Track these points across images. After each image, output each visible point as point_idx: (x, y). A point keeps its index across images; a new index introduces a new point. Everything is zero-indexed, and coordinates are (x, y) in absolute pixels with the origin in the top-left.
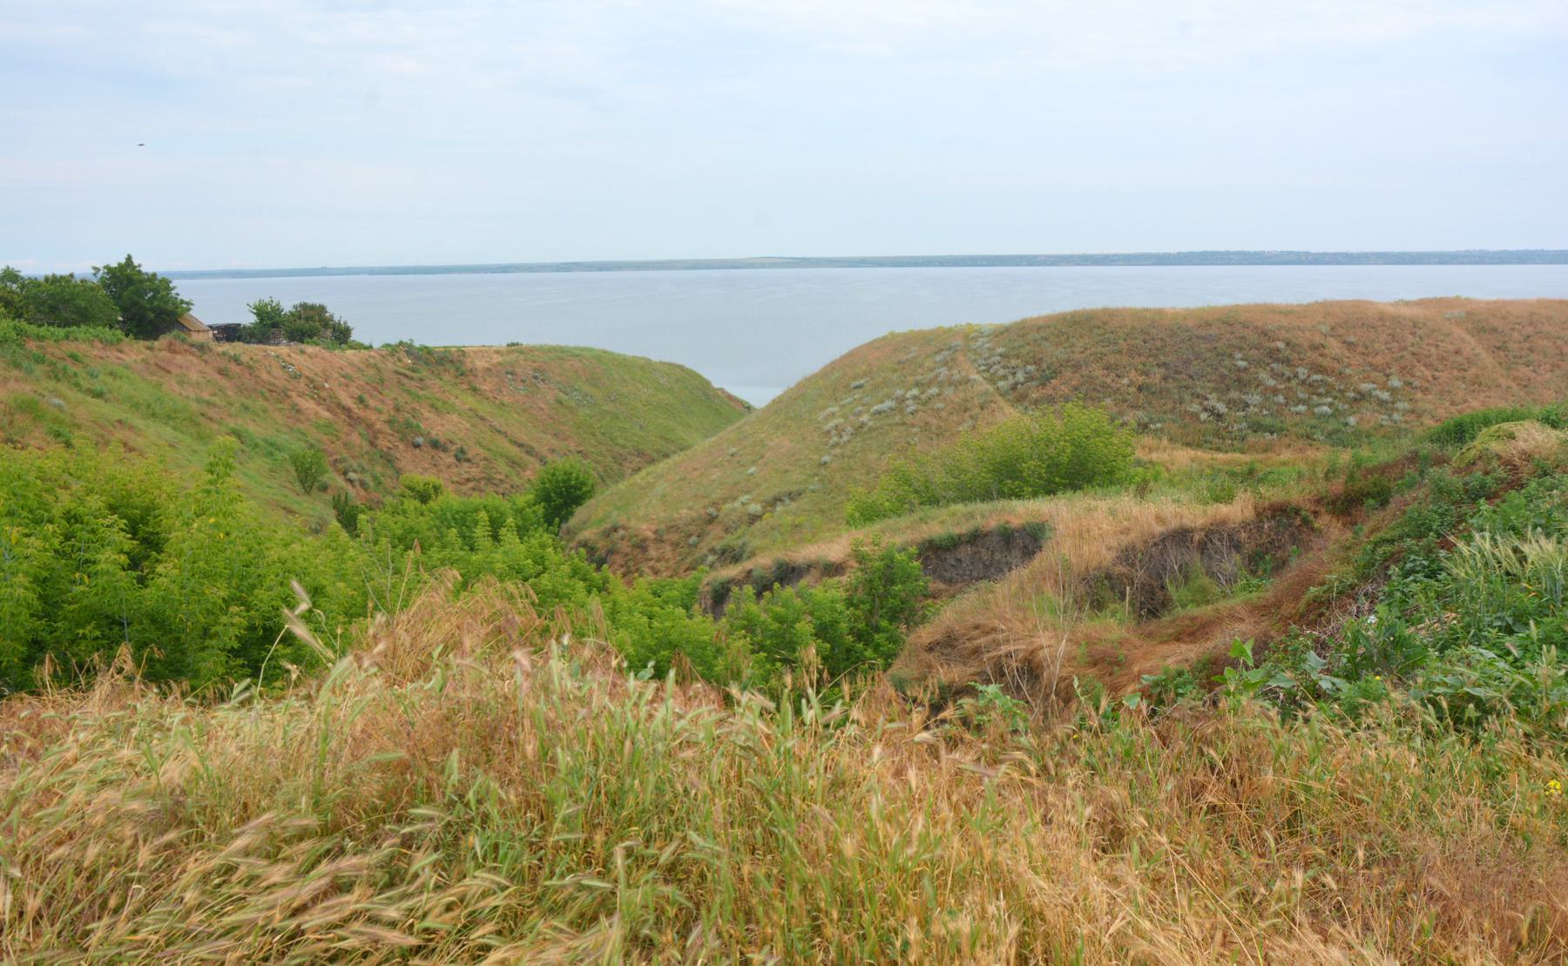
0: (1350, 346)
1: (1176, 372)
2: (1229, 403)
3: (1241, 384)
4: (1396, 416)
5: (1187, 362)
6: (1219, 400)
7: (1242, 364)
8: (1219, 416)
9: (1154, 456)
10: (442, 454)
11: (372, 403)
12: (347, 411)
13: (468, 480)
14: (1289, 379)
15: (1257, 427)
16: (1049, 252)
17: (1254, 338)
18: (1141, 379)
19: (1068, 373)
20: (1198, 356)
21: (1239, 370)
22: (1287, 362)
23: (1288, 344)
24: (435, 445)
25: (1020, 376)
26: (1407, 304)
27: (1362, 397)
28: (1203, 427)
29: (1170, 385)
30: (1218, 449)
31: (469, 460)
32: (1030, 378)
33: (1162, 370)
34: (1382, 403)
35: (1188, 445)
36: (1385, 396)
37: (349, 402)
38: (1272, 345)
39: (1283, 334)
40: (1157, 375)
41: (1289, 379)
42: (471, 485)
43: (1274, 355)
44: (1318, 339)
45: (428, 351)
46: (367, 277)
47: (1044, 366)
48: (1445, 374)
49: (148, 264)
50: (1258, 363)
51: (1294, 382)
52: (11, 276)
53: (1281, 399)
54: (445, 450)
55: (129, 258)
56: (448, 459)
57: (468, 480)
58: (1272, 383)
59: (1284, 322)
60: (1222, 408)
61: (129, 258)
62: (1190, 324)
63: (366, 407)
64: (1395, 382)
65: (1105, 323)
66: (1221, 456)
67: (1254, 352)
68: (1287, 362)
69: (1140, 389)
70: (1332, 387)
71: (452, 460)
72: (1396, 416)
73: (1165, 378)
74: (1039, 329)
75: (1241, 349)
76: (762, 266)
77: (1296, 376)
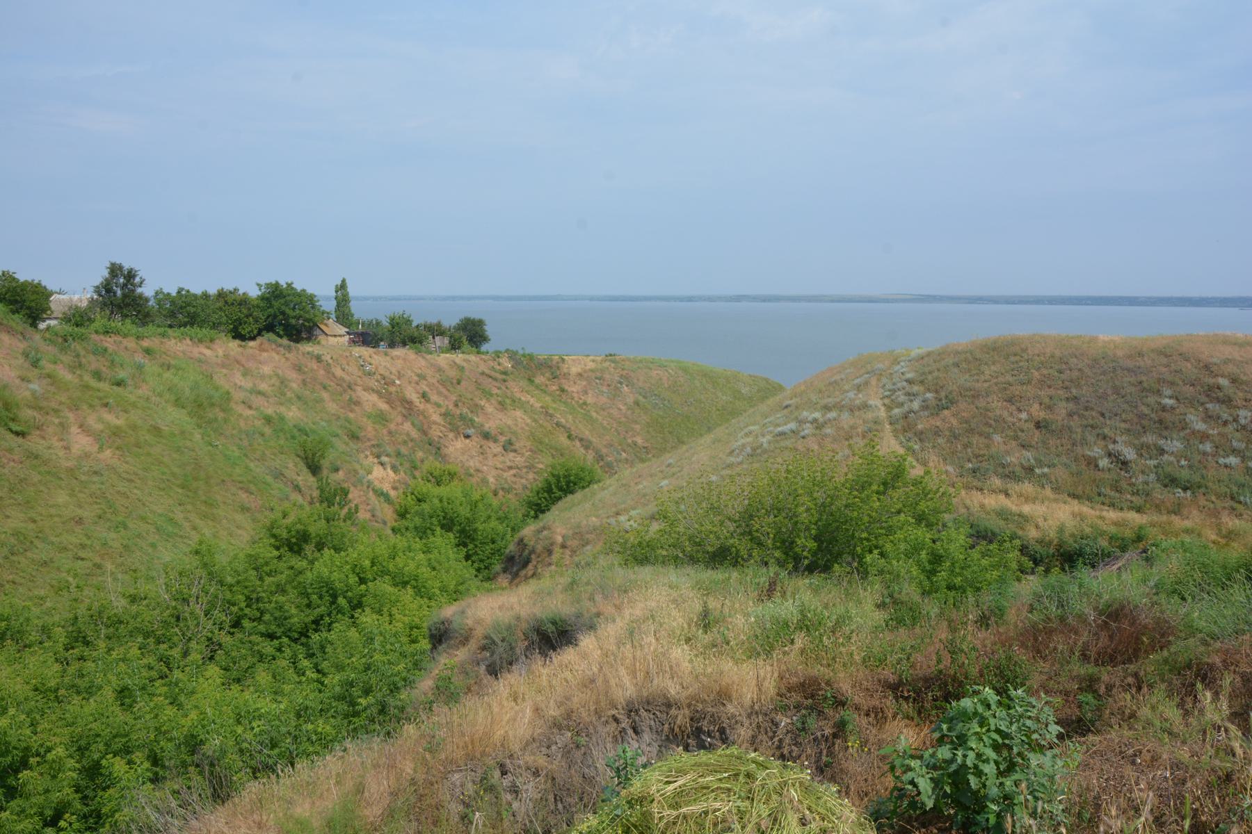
1: (1086, 409)
2: (1141, 449)
3: (1163, 426)
5: (1104, 396)
6: (1130, 444)
7: (1169, 402)
9: (1026, 509)
10: (491, 444)
11: (434, 398)
12: (408, 404)
13: (510, 468)
14: (1225, 423)
15: (1171, 481)
16: (1168, 295)
18: (1042, 415)
19: (962, 405)
20: (1116, 390)
21: (1164, 409)
22: (1227, 401)
23: (1234, 381)
24: (486, 436)
25: (916, 405)
26: (1226, 341)
28: (1099, 475)
29: (1075, 423)
30: (1112, 505)
31: (515, 451)
32: (925, 407)
33: (1071, 406)
35: (1074, 496)
37: (414, 397)
38: (1211, 381)
39: (1231, 368)
40: (1062, 408)
41: (1225, 423)
42: (512, 472)
43: (1212, 392)
45: (531, 357)
47: (943, 394)
50: (1192, 403)
51: (1230, 428)
52: (8, 277)
53: (1208, 447)
54: (495, 441)
55: (344, 281)
56: (497, 449)
57: (510, 468)
58: (1200, 426)
60: (1129, 454)
61: (344, 281)
62: (1120, 353)
63: (428, 401)
65: (1024, 350)
66: (1112, 515)
67: (1189, 390)
68: (1227, 401)
69: (1038, 425)
71: (500, 449)
73: (1070, 415)
74: (957, 353)
75: (1172, 384)
77: (1235, 420)
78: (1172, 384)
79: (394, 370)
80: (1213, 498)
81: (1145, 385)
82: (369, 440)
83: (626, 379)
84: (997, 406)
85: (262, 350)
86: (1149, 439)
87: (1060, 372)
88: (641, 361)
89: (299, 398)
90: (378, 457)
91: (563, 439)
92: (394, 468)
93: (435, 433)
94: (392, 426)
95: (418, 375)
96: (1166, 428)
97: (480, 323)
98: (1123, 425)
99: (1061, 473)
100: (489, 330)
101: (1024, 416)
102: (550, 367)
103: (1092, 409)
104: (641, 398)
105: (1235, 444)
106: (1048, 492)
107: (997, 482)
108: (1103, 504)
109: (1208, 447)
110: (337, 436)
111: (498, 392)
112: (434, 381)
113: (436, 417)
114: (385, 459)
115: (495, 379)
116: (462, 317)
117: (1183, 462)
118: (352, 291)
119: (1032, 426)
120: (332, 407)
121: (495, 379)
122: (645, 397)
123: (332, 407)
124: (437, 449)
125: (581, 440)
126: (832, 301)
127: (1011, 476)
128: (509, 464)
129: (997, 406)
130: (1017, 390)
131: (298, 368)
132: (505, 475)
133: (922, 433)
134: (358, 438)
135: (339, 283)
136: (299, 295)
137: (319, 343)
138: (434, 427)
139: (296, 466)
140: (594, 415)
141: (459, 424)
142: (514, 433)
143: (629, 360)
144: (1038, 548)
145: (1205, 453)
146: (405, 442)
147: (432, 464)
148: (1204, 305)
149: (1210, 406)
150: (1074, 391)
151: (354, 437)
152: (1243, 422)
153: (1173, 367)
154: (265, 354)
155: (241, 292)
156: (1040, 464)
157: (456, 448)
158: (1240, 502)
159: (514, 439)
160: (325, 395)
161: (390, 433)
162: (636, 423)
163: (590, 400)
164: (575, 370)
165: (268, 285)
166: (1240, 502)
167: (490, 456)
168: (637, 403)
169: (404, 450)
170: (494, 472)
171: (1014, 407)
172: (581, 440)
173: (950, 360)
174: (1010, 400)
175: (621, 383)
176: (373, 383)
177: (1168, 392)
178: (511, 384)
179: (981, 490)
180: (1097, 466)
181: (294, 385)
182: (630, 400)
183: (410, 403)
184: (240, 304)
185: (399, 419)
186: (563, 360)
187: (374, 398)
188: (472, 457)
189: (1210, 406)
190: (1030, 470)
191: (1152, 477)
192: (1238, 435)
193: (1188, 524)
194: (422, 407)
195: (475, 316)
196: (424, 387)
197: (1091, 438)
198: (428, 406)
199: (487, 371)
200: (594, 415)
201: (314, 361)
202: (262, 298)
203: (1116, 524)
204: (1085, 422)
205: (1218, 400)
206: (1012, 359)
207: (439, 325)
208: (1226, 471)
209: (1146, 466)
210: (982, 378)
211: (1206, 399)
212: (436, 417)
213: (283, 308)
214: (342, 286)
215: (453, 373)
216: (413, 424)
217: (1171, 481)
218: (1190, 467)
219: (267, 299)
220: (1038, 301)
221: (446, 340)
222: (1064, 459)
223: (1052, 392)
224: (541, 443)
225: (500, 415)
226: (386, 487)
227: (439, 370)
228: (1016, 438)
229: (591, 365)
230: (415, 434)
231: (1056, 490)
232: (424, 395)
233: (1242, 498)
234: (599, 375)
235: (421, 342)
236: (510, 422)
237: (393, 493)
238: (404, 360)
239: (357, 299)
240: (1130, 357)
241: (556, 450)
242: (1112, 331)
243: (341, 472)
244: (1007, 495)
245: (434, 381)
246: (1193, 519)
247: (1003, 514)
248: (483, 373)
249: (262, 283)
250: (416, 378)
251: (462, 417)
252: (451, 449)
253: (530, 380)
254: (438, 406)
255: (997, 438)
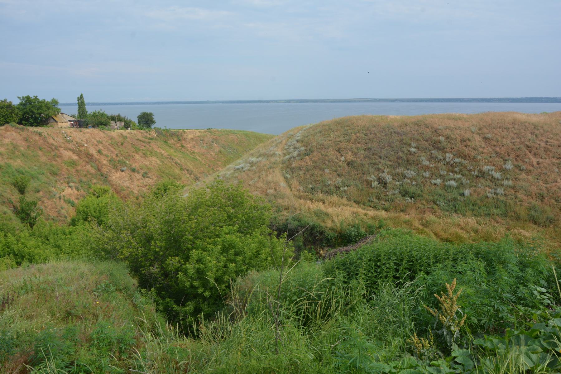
0: (486, 139)
1: (373, 154)
2: (395, 176)
3: (408, 163)
4: (500, 191)
7: (413, 150)
8: (385, 184)
9: (330, 210)
10: (136, 174)
11: (105, 152)
13: (146, 185)
15: (405, 193)
17: (428, 133)
18: (352, 158)
21: (411, 153)
22: (443, 150)
23: (447, 138)
24: (133, 170)
25: (295, 154)
27: (482, 175)
30: (374, 207)
31: (149, 177)
33: (366, 153)
34: (493, 179)
35: (357, 203)
36: (498, 175)
37: (93, 151)
38: (435, 138)
39: (448, 132)
43: (436, 145)
44: (467, 135)
45: (167, 131)
46: (221, 104)
47: (309, 147)
48: (547, 161)
49: (32, 96)
50: (425, 150)
53: (428, 174)
54: (138, 173)
55: (82, 95)
56: (139, 176)
58: (426, 163)
59: (452, 124)
60: (389, 178)
61: (82, 95)
62: (396, 125)
64: (509, 166)
65: (353, 124)
68: (443, 150)
70: (465, 167)
72: (500, 191)
75: (417, 140)
76: (359, 101)
78: (417, 140)
79: (84, 139)
80: (425, 203)
81: (404, 141)
82: (63, 175)
83: (216, 140)
84: (331, 153)
85: (6, 130)
86: (400, 170)
87: (366, 135)
88: (224, 131)
89: (23, 155)
90: (68, 183)
91: (177, 171)
92: (77, 189)
93: (105, 170)
94: (79, 168)
95: (98, 141)
96: (410, 164)
97: (150, 115)
98: (389, 163)
99: (352, 190)
100: (155, 118)
101: (343, 159)
102: (177, 135)
103: (376, 154)
104: (222, 149)
105: (441, 172)
106: (344, 200)
107: (321, 195)
108: (370, 206)
109: (428, 174)
110: (43, 174)
111: (144, 148)
112: (107, 144)
113: (105, 162)
114: (71, 184)
115: (144, 142)
116: (142, 112)
117: (414, 183)
118: (86, 100)
119: (345, 164)
120: (44, 159)
121: (144, 142)
122: (224, 149)
123: (44, 159)
124: (105, 178)
125: (188, 170)
126: (332, 102)
127: (328, 192)
128: (145, 184)
129: (331, 153)
130: (343, 145)
131: (26, 140)
132: (144, 189)
133: (294, 168)
134: (56, 174)
135: (79, 96)
136: (41, 102)
137: (51, 126)
138: (104, 167)
139: (11, 191)
140: (198, 157)
141: (117, 165)
142: (149, 169)
143: (218, 131)
144: (330, 233)
145: (426, 178)
146: (86, 176)
147: (99, 186)
148: (492, 102)
149: (433, 152)
150: (370, 145)
151: (54, 174)
152: (448, 160)
153: (421, 131)
154: (8, 133)
155: (8, 101)
156: (344, 185)
157: (116, 177)
158: (437, 205)
159: (148, 172)
160: (40, 153)
161: (77, 171)
162: (219, 161)
163: (196, 151)
164: (190, 136)
165: (23, 98)
166: (437, 205)
167: (135, 180)
168: (220, 152)
169: (84, 179)
170: (137, 188)
171: (340, 154)
172: (188, 170)
173: (319, 130)
174: (339, 151)
175: (213, 142)
176: (70, 146)
177: (414, 144)
178: (153, 144)
179: (312, 200)
180: (371, 185)
181: (22, 149)
182: (217, 150)
183: (92, 155)
184: (7, 107)
185: (84, 163)
186: (185, 132)
187: (70, 153)
188: (126, 181)
189: (433, 152)
190: (338, 188)
191: (397, 191)
192: (444, 167)
193: (407, 218)
194: (98, 157)
195: (148, 111)
196: (100, 147)
197: (372, 170)
198: (101, 156)
199: (141, 138)
200: (198, 157)
201: (37, 136)
202: (21, 104)
203: (373, 218)
204: (371, 162)
205: (438, 149)
206: (346, 128)
207: (119, 116)
208: (433, 187)
209: (395, 185)
210: (329, 139)
211: (433, 148)
212: (105, 162)
213: (32, 109)
214: (81, 98)
215: (120, 139)
216: (92, 166)
217: (405, 193)
218: (417, 185)
219: (24, 105)
220: (158, 103)
221: (123, 124)
222: (357, 182)
223: (359, 145)
224: (164, 173)
225: (143, 160)
226: (73, 199)
227: (112, 138)
228: (336, 171)
229: (198, 134)
230: (93, 171)
231: (349, 199)
232: (99, 152)
233: (438, 202)
234: (202, 138)
235: (106, 125)
236: (147, 163)
237: (76, 201)
238: (91, 134)
239: (89, 104)
240: (400, 127)
241: (172, 176)
242: (395, 115)
243: (41, 193)
244: (324, 203)
245: (107, 144)
246: (412, 216)
247: (318, 214)
248: (138, 140)
249: (21, 96)
250: (96, 143)
251: (119, 162)
252: (114, 178)
253: (166, 142)
254: (107, 156)
255: (327, 171)
